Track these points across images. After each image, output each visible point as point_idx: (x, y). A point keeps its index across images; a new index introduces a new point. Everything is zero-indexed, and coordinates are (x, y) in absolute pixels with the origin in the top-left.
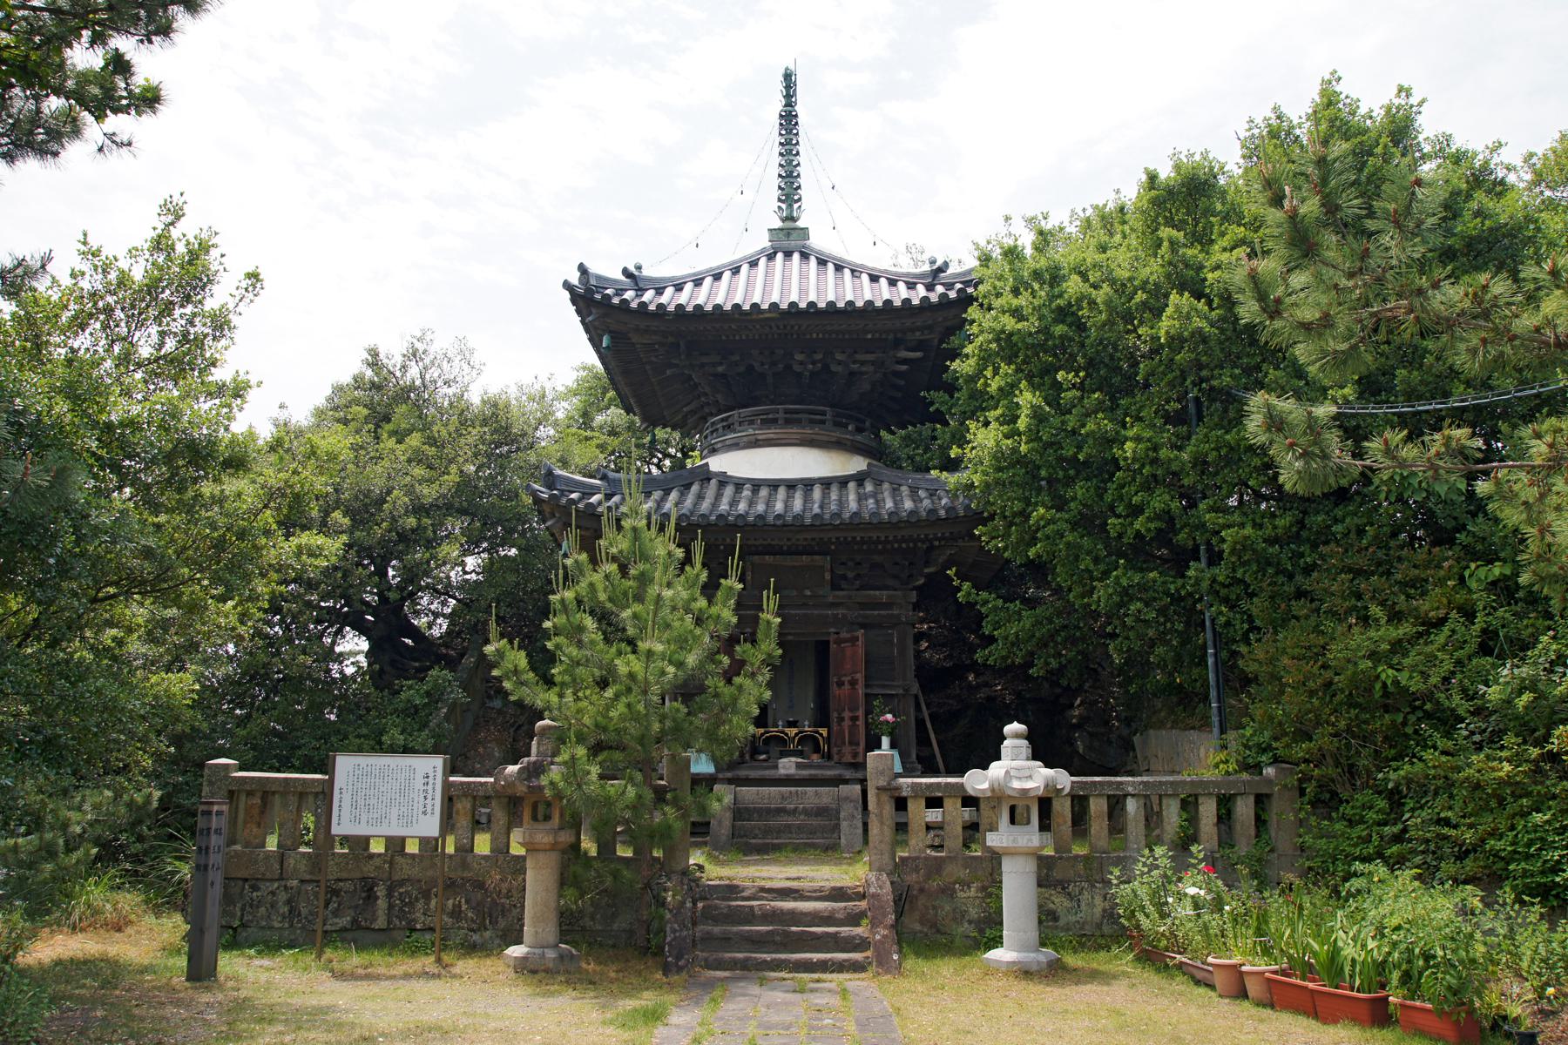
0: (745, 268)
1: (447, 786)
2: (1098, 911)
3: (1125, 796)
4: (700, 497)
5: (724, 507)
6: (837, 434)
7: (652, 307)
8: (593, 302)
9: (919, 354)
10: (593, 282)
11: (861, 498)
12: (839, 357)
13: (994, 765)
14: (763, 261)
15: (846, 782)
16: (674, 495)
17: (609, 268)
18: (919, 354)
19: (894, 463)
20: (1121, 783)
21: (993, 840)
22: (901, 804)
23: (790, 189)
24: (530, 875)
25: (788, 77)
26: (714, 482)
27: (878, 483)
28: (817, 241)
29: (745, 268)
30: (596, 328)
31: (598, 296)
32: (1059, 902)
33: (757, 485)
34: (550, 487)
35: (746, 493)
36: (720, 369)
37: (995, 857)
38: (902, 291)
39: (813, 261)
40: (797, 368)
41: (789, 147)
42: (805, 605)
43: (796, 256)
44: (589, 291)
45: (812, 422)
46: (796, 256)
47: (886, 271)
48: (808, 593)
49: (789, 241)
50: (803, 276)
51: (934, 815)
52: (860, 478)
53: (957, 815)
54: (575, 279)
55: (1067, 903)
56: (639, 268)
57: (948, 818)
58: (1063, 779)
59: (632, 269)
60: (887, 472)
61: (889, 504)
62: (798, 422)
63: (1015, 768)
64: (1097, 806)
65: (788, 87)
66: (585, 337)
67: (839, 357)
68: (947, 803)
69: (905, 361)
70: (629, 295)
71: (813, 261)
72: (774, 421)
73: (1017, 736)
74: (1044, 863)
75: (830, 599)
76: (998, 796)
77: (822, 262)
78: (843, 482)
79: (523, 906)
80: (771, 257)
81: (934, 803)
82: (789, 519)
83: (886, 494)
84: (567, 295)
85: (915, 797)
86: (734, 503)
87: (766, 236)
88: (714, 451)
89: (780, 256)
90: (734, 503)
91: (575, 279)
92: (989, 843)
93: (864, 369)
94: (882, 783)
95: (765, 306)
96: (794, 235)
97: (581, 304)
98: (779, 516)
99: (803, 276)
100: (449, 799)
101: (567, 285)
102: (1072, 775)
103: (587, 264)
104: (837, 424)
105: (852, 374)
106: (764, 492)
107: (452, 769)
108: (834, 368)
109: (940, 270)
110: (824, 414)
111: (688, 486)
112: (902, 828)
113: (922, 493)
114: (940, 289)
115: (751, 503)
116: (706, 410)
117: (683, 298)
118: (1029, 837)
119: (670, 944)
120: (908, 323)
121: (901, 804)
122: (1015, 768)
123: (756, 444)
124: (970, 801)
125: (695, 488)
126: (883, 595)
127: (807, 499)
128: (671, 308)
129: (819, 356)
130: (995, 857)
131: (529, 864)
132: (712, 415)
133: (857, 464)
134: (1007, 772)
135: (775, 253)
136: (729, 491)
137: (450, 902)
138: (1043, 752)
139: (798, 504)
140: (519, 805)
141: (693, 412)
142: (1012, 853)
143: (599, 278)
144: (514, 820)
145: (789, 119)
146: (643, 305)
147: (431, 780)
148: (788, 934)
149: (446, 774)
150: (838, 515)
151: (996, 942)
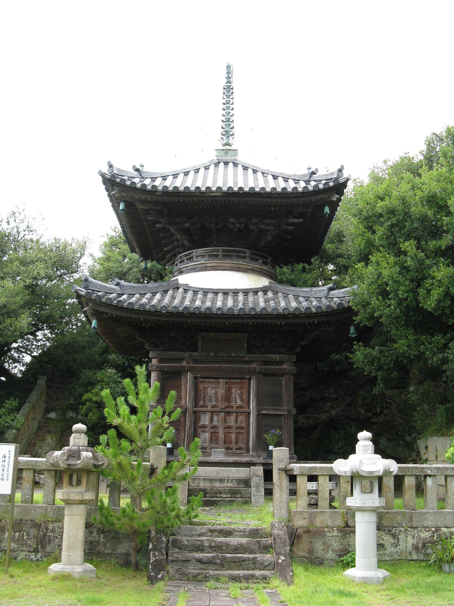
0: (202, 170)
1: (16, 462)
2: (410, 545)
3: (425, 476)
4: (173, 298)
5: (187, 303)
6: (253, 265)
7: (149, 187)
8: (117, 187)
9: (301, 220)
10: (115, 171)
11: (267, 301)
12: (254, 221)
13: (351, 457)
14: (212, 167)
15: (254, 464)
16: (158, 296)
17: (125, 166)
18: (301, 220)
19: (281, 282)
20: (423, 468)
21: (351, 502)
22: (293, 478)
23: (228, 131)
24: (67, 520)
25: (228, 67)
26: (181, 290)
27: (276, 293)
28: (242, 158)
29: (202, 170)
30: (116, 199)
31: (118, 180)
32: (388, 540)
33: (206, 292)
34: (86, 288)
35: (200, 296)
36: (186, 225)
37: (351, 513)
38: (291, 185)
39: (240, 167)
40: (230, 226)
41: (228, 105)
42: (231, 362)
43: (231, 165)
44: (114, 176)
45: (238, 257)
46: (231, 165)
47: (282, 173)
48: (234, 355)
49: (226, 158)
50: (235, 175)
51: (312, 486)
52: (265, 290)
53: (324, 485)
54: (106, 170)
55: (391, 540)
56: (142, 166)
57: (321, 488)
58: (392, 465)
59: (138, 167)
60: (280, 287)
61: (283, 304)
62: (230, 257)
63: (365, 458)
64: (409, 482)
65: (228, 73)
66: (110, 204)
67: (254, 221)
68: (321, 479)
69: (292, 224)
70: (136, 180)
71: (240, 167)
72: (217, 256)
73: (366, 439)
74: (380, 517)
75: (246, 359)
76: (354, 477)
77: (245, 168)
78: (255, 292)
79: (62, 538)
80: (217, 164)
81: (312, 478)
82: (225, 311)
83: (280, 299)
84: (101, 179)
85: (302, 475)
86: (193, 301)
87: (215, 153)
88: (181, 272)
89: (222, 164)
90: (193, 301)
91: (106, 170)
92: (348, 504)
93: (268, 228)
94: (282, 466)
95: (214, 189)
96: (230, 153)
97: (109, 185)
98: (219, 309)
99: (235, 175)
100: (19, 473)
101: (102, 175)
102: (398, 463)
103: (113, 163)
104: (252, 259)
105: (261, 231)
106: (210, 296)
107: (22, 452)
108: (252, 227)
109: (313, 173)
110: (245, 252)
111: (166, 292)
112: (293, 492)
113: (301, 299)
114: (313, 183)
115: (203, 302)
116: (177, 250)
117: (168, 183)
118: (373, 500)
119: (152, 564)
120: (295, 200)
121: (293, 478)
122: (365, 458)
123: (205, 269)
124: (334, 477)
125: (170, 293)
126: (277, 357)
127: (235, 301)
128: (160, 188)
129: (242, 220)
130: (351, 513)
131: (66, 512)
132: (180, 253)
133: (264, 282)
134: (361, 461)
135: (219, 163)
136: (190, 294)
137: (17, 534)
138: (380, 450)
139: (230, 303)
140: (62, 476)
141: (169, 251)
142: (361, 510)
143: (119, 170)
144: (58, 484)
145: (228, 89)
146: (144, 185)
147: (7, 459)
148: (224, 559)
149: (16, 456)
150: (253, 309)
151: (351, 564)
